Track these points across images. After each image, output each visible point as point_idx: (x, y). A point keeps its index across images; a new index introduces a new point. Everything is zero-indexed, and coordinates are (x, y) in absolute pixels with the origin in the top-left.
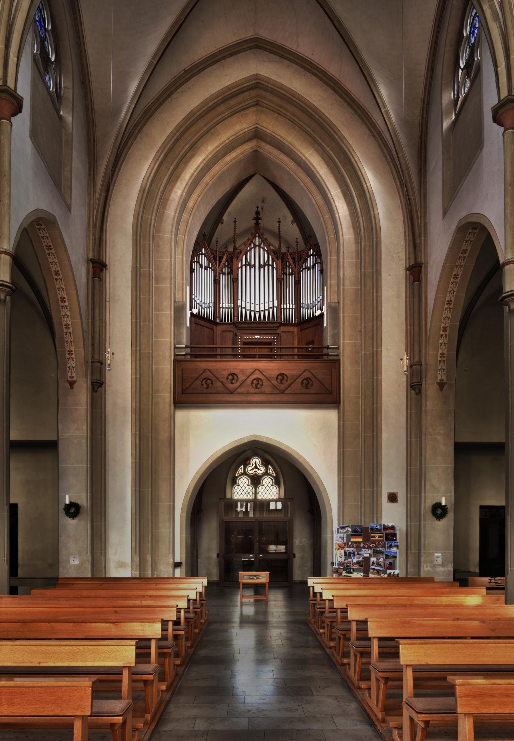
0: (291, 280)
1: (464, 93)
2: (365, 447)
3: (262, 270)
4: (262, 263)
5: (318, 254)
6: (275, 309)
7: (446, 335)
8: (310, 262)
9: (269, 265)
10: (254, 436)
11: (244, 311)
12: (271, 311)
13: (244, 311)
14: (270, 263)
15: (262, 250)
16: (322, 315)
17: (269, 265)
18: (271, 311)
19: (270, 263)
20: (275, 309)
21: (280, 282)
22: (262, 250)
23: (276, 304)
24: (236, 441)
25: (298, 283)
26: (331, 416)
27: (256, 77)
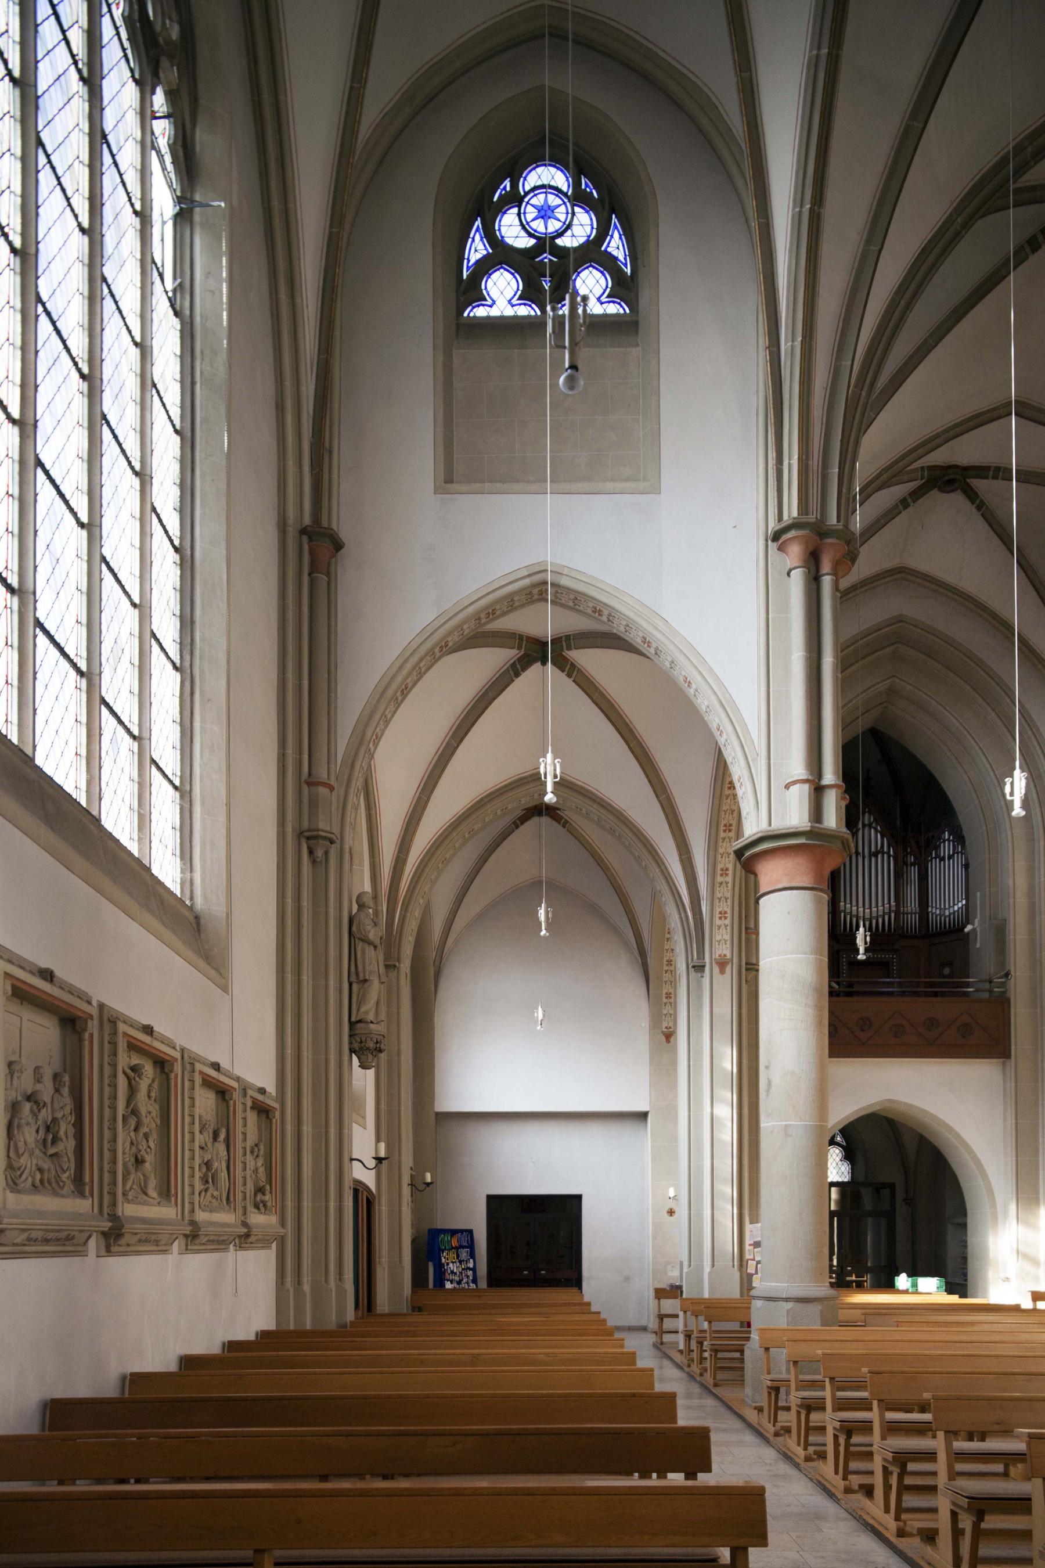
0: (914, 873)
1: (468, 268)
2: (327, 1215)
3: (873, 859)
4: (873, 850)
5: (960, 839)
6: (893, 915)
7: (726, 926)
8: (946, 849)
9: (883, 853)
10: (890, 1101)
11: (848, 917)
12: (886, 917)
13: (848, 917)
14: (885, 849)
15: (873, 831)
16: (974, 930)
17: (883, 853)
18: (886, 917)
19: (885, 849)
20: (893, 915)
21: (898, 875)
22: (873, 831)
23: (893, 908)
24: (864, 1108)
25: (923, 878)
26: (437, 1110)
27: (900, 620)
